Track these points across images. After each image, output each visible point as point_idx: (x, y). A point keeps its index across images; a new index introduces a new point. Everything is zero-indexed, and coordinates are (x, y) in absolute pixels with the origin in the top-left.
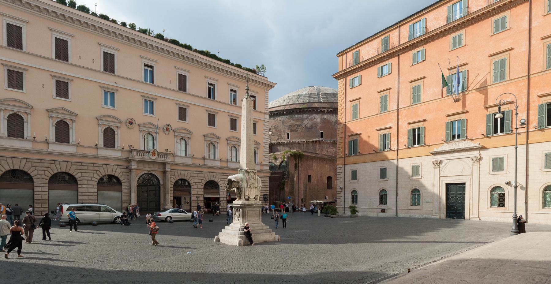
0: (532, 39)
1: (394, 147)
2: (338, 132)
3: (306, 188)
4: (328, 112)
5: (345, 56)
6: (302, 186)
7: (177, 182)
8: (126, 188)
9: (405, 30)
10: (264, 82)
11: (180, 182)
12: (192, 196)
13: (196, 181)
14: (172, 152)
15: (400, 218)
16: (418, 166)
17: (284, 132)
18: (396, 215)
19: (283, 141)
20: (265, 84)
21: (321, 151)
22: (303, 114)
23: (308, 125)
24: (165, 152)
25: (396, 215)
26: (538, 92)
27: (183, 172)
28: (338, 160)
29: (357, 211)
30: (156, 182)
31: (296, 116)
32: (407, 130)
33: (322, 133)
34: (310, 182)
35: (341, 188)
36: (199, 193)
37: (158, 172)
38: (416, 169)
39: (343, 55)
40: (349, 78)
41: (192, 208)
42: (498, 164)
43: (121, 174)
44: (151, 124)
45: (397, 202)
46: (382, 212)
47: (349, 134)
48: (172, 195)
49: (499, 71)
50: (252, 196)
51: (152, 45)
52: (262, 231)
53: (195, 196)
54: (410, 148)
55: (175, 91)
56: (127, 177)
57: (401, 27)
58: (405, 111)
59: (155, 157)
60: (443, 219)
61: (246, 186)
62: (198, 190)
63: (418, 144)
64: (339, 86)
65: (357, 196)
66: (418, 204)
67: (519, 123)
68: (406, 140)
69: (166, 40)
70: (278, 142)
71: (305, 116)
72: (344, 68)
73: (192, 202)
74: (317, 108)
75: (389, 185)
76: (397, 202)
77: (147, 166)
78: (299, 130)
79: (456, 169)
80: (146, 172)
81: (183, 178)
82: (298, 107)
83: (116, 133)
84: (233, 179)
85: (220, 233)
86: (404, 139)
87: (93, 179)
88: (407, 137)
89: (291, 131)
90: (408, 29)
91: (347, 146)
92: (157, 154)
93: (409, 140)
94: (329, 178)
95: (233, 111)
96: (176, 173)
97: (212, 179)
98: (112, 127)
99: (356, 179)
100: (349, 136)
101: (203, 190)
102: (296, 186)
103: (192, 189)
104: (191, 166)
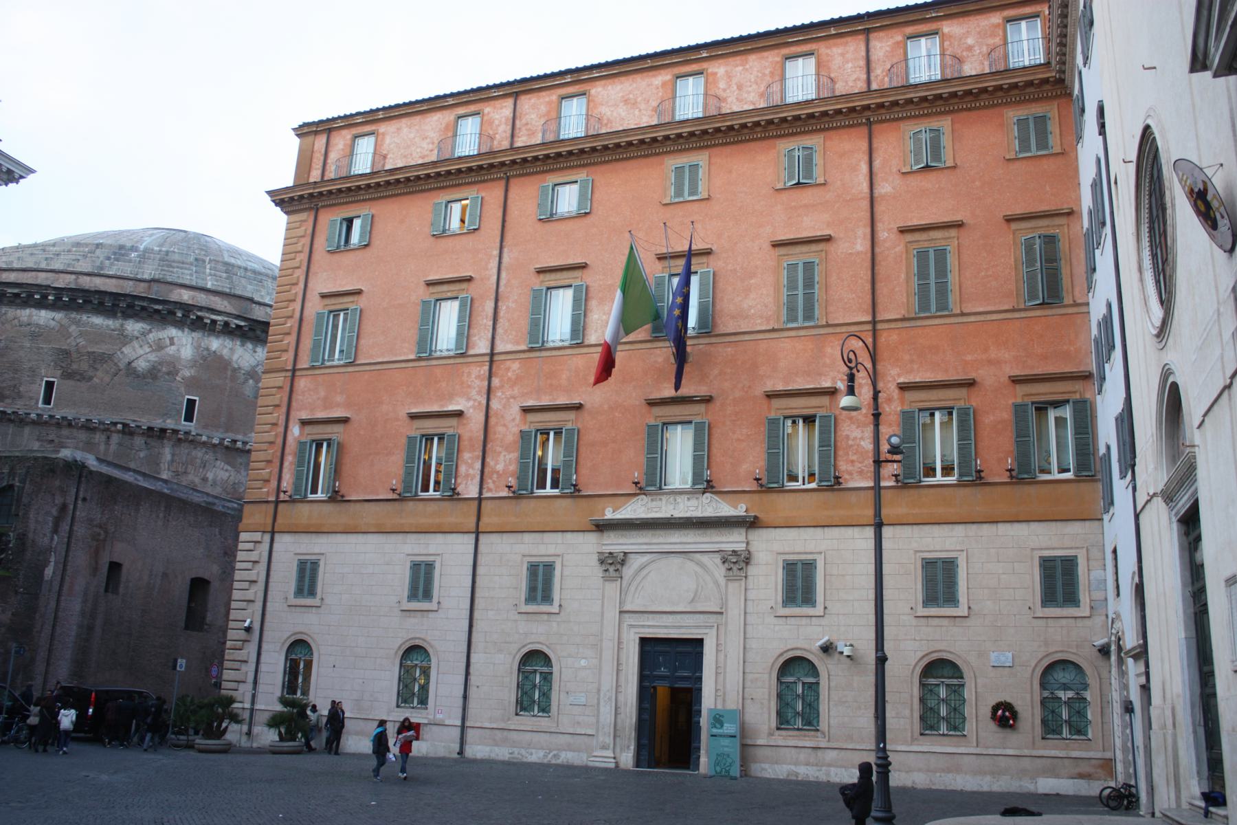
0: (879, 226)
4: (227, 331)
6: (74, 607)
17: (33, 372)
18: (461, 753)
21: (177, 474)
23: (142, 365)
25: (461, 753)
26: (899, 375)
28: (247, 509)
31: (98, 320)
32: (516, 430)
33: (191, 403)
34: (116, 591)
42: (799, 584)
45: (465, 697)
47: (305, 415)
49: (800, 292)
58: (515, 366)
60: (627, 771)
65: (309, 665)
66: (543, 710)
67: (885, 447)
71: (134, 327)
74: (187, 308)
79: (673, 588)
82: (111, 286)
88: (515, 455)
89: (68, 375)
91: (289, 459)
100: (304, 423)
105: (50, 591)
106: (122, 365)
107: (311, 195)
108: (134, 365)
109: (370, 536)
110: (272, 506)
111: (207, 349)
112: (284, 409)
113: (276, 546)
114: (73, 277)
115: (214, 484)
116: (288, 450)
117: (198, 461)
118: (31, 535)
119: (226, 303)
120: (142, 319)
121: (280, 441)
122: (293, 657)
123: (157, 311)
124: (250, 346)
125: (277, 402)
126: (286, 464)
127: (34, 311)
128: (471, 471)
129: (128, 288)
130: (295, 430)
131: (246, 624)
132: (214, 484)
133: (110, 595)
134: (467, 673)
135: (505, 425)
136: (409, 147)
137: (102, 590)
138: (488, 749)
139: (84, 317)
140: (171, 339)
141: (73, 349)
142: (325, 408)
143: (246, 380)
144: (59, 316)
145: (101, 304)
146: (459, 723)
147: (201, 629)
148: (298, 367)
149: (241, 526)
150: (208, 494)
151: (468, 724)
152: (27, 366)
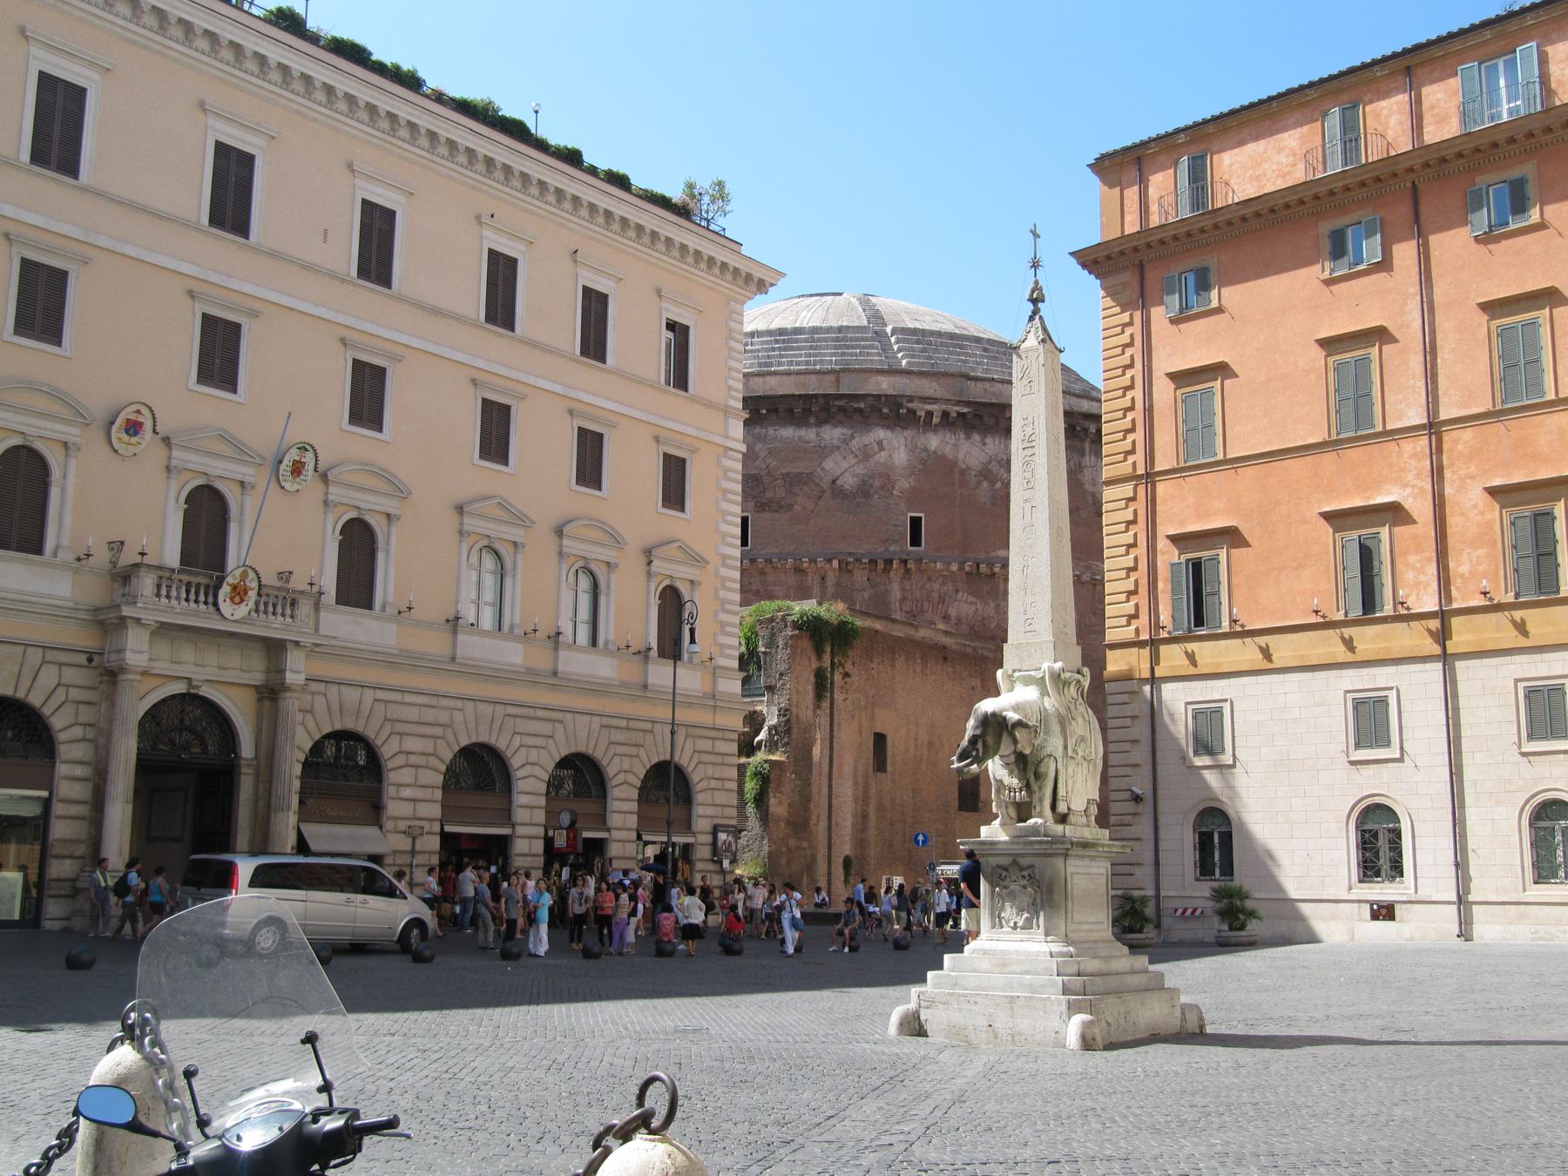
3: (865, 801)
6: (846, 792)
7: (317, 748)
8: (79, 771)
11: (330, 751)
13: (411, 744)
22: (820, 423)
27: (352, 695)
29: (1252, 914)
31: (788, 432)
33: (916, 522)
35: (1137, 799)
37: (236, 693)
43: (61, 695)
46: (1375, 916)
53: (402, 825)
56: (86, 714)
59: (242, 611)
61: (1059, 753)
62: (419, 793)
69: (314, 39)
71: (832, 434)
74: (894, 401)
77: (187, 653)
81: (350, 725)
84: (1013, 716)
87: (434, 762)
91: (1163, 586)
92: (253, 595)
97: (483, 738)
98: (218, 485)
99: (1383, 740)
101: (438, 794)
103: (392, 791)
104: (391, 662)
106: (825, 485)
111: (926, 450)
117: (936, 595)
119: (935, 385)
120: (841, 423)
123: (860, 411)
124: (976, 437)
128: (1422, 578)
129: (813, 387)
135: (1463, 514)
136: (1259, 165)
139: (771, 431)
140: (880, 443)
141: (763, 473)
142: (1199, 518)
143: (979, 483)
145: (790, 411)
151: (1163, 893)
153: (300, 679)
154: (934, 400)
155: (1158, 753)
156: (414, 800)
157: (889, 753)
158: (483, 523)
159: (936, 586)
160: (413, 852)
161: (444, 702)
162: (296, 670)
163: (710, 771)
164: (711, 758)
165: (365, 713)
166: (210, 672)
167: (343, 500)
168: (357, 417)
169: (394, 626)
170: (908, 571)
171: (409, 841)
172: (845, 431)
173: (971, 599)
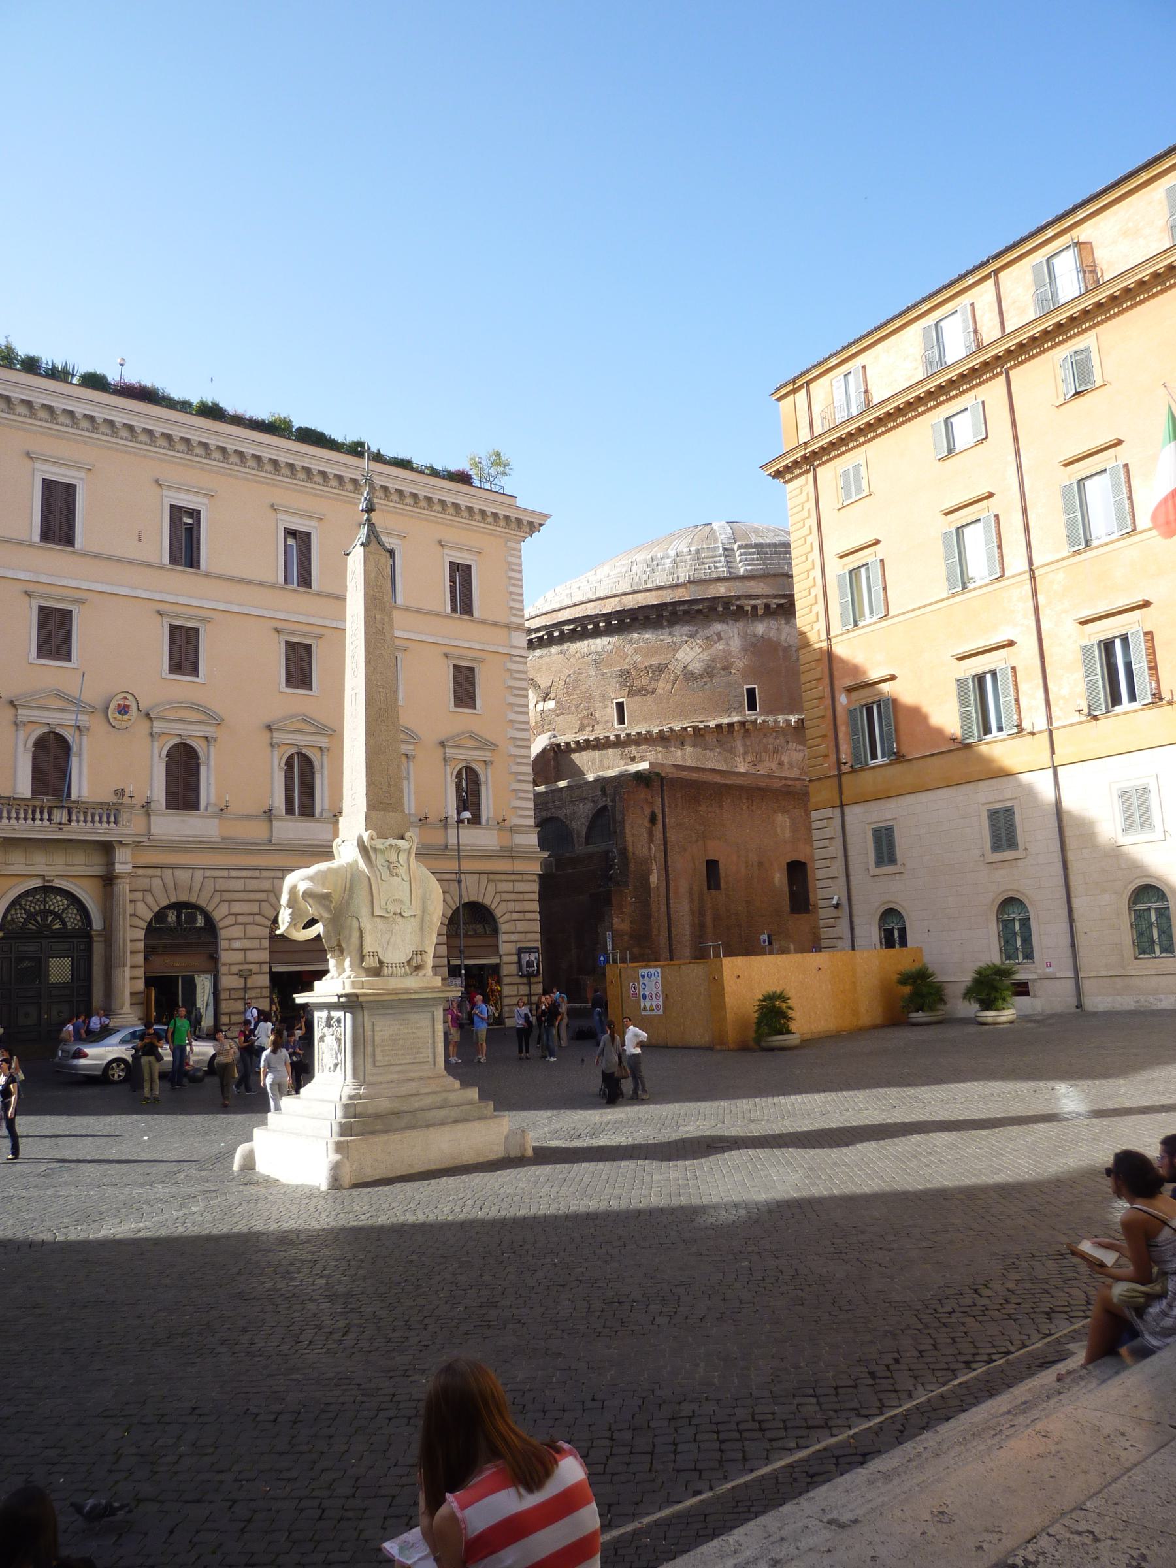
1: (1034, 718)
2: (803, 678)
3: (702, 913)
4: (769, 612)
5: (802, 393)
6: (683, 909)
7: (160, 916)
9: (1018, 281)
10: (502, 512)
11: (172, 917)
12: (223, 970)
13: (237, 908)
14: (139, 800)
15: (1095, 1014)
16: (1143, 791)
17: (604, 698)
19: (600, 733)
20: (507, 518)
23: (696, 667)
24: (113, 799)
25: (1079, 1006)
27: (183, 876)
30: (73, 920)
33: (751, 692)
34: (718, 887)
36: (253, 956)
37: (85, 883)
38: (1137, 806)
39: (795, 391)
40: (828, 473)
41: (224, 1019)
44: (59, 695)
45: (1073, 945)
48: (140, 972)
50: (397, 954)
51: (71, 414)
52: (443, 1113)
53: (235, 969)
54: (1095, 718)
55: (443, 616)
57: (1001, 275)
62: (247, 944)
63: (1133, 697)
64: (790, 504)
68: (1081, 688)
70: (581, 738)
72: (805, 436)
73: (223, 996)
74: (726, 601)
75: (1033, 874)
76: (1073, 945)
78: (662, 686)
80: (37, 883)
81: (184, 898)
82: (652, 599)
83: (482, 779)
85: (257, 1132)
86: (1073, 684)
87: (259, 919)
89: (630, 693)
90: (1029, 278)
91: (843, 730)
93: (1091, 686)
94: (797, 871)
95: (297, 610)
96: (157, 882)
98: (59, 730)
100: (850, 690)
102: (658, 906)
103: (223, 944)
105: (659, 896)
107: (805, 457)
108: (690, 668)
109: (939, 792)
110: (835, 780)
111: (755, 636)
112: (827, 681)
113: (848, 819)
114: (617, 599)
115: (791, 766)
116: (839, 721)
117: (771, 747)
118: (630, 849)
119: (762, 585)
120: (687, 623)
121: (829, 713)
122: (887, 927)
123: (699, 611)
125: (819, 676)
126: (841, 735)
127: (591, 641)
129: (668, 596)
130: (843, 699)
131: (834, 902)
132: (791, 766)
133: (713, 892)
134: (1071, 920)
137: (705, 888)
138: (1109, 999)
144: (614, 640)
145: (647, 618)
146: (1071, 974)
147: (807, 911)
148: (832, 634)
149: (811, 806)
150: (786, 778)
152: (596, 693)
153: (128, 868)
154: (757, 597)
155: (851, 867)
156: (245, 950)
157: (722, 875)
158: (290, 736)
159: (771, 740)
160: (245, 989)
161: (265, 874)
162: (123, 863)
163: (511, 906)
164: (513, 896)
165: (197, 887)
166: (59, 869)
167: (166, 731)
168: (175, 667)
169: (216, 821)
170: (747, 731)
171: (242, 980)
172: (691, 628)
173: (800, 747)
